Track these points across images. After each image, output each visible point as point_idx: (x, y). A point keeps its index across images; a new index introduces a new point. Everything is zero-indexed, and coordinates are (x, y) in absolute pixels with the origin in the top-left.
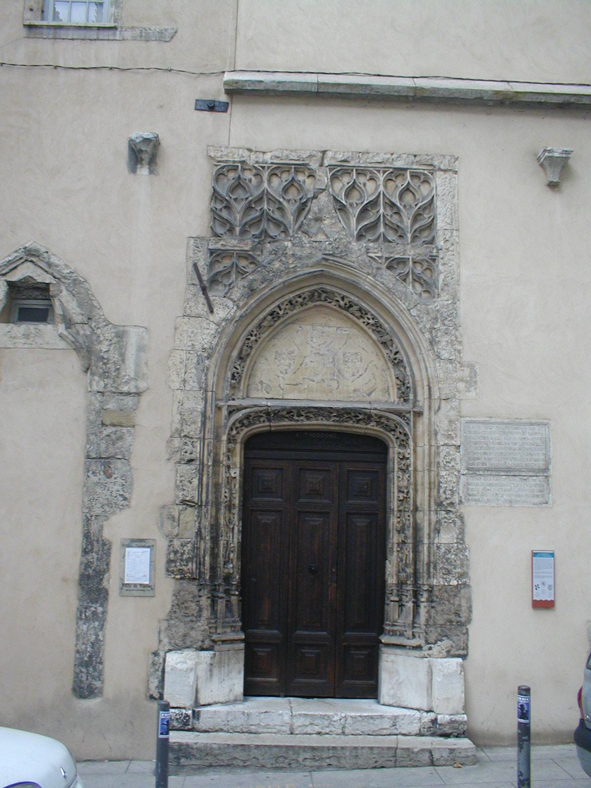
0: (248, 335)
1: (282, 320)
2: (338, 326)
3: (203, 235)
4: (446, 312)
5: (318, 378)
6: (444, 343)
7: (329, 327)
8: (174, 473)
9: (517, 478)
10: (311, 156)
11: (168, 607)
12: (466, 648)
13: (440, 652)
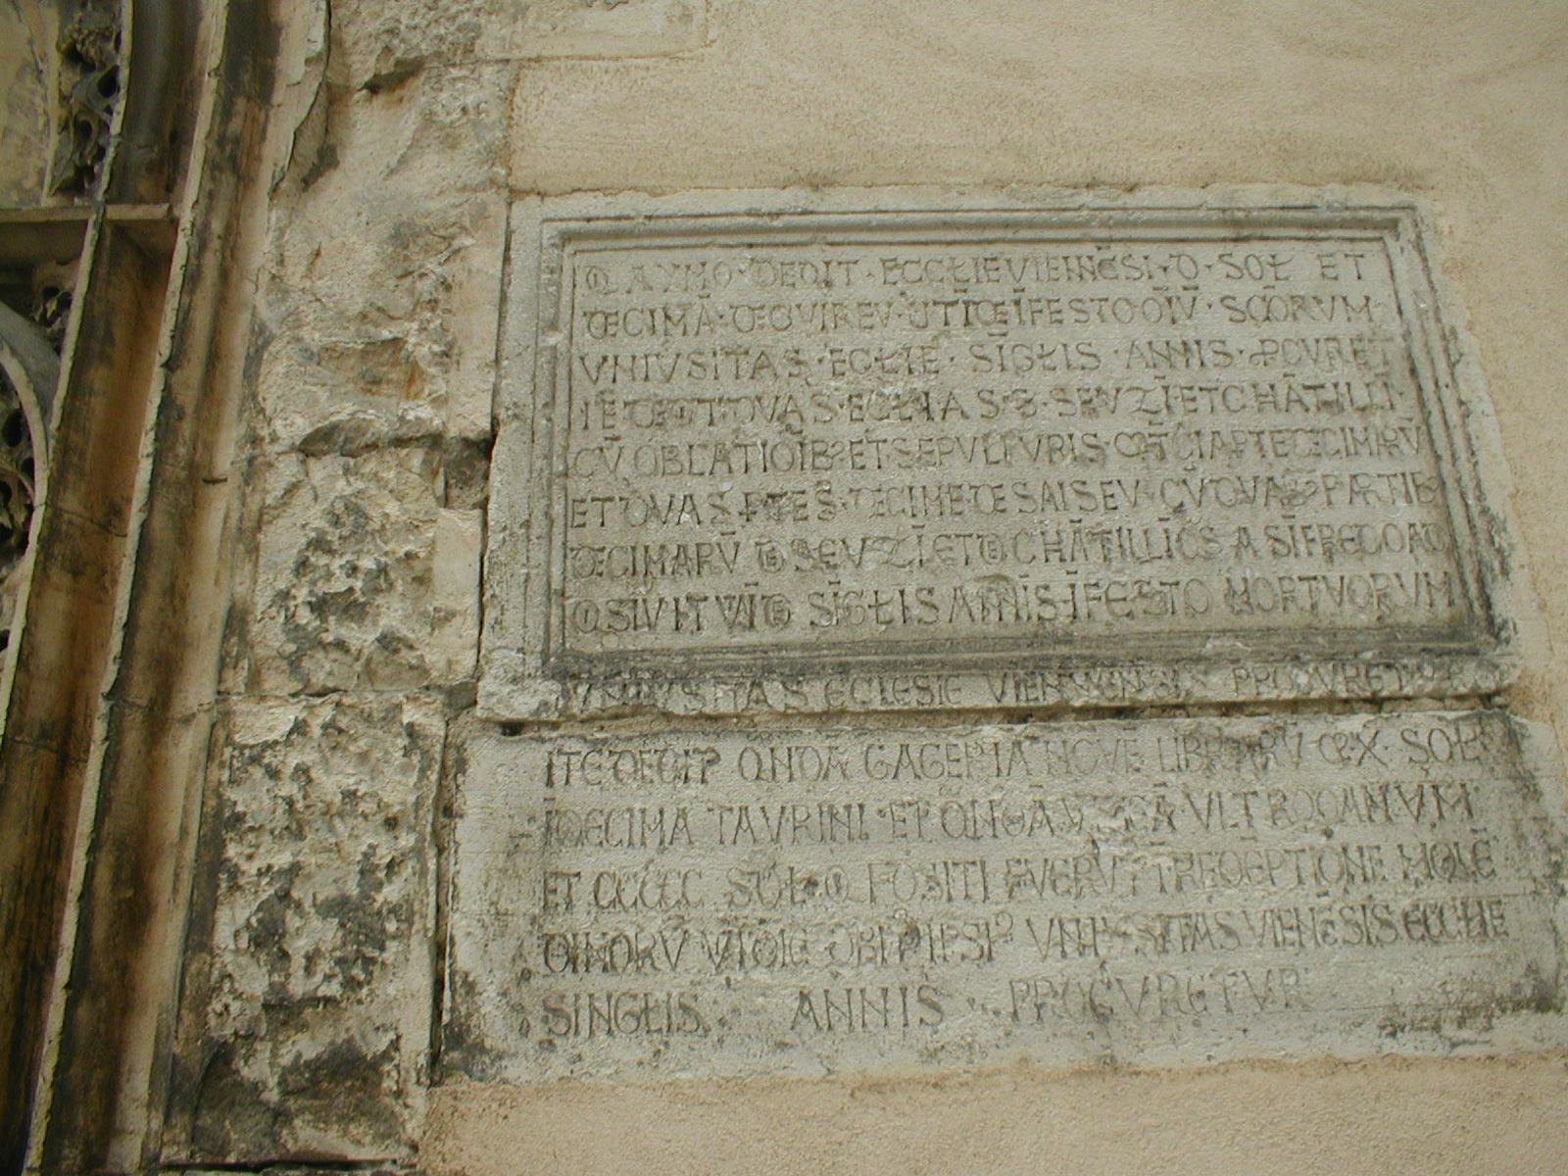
9: (1149, 734)
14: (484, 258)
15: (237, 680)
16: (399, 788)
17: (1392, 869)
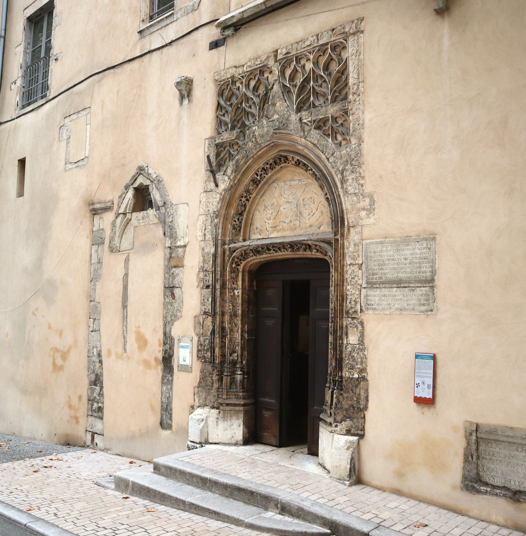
0: (240, 198)
1: (262, 182)
2: (300, 179)
3: (212, 136)
4: (353, 154)
5: (287, 221)
6: (350, 181)
7: (294, 181)
8: (200, 294)
9: (406, 289)
10: (268, 57)
11: (198, 379)
12: (363, 429)
13: (341, 430)
14: (361, 247)
15: (347, 284)
16: (357, 293)
17: (422, 300)
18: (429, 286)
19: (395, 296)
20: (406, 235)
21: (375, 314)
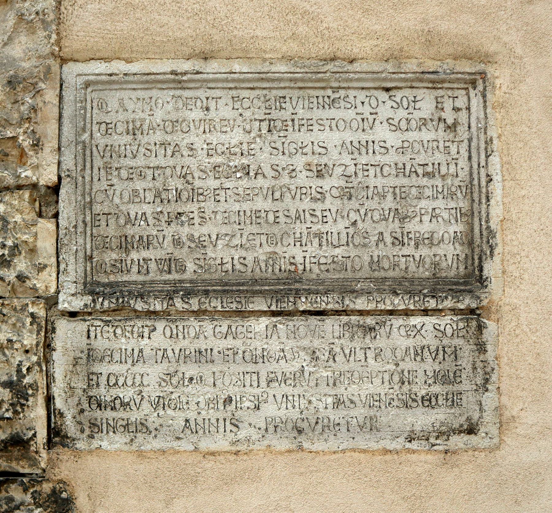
14: (51, 96)
18: (454, 311)
19: (264, 357)
20: (325, 49)
21: (140, 454)
